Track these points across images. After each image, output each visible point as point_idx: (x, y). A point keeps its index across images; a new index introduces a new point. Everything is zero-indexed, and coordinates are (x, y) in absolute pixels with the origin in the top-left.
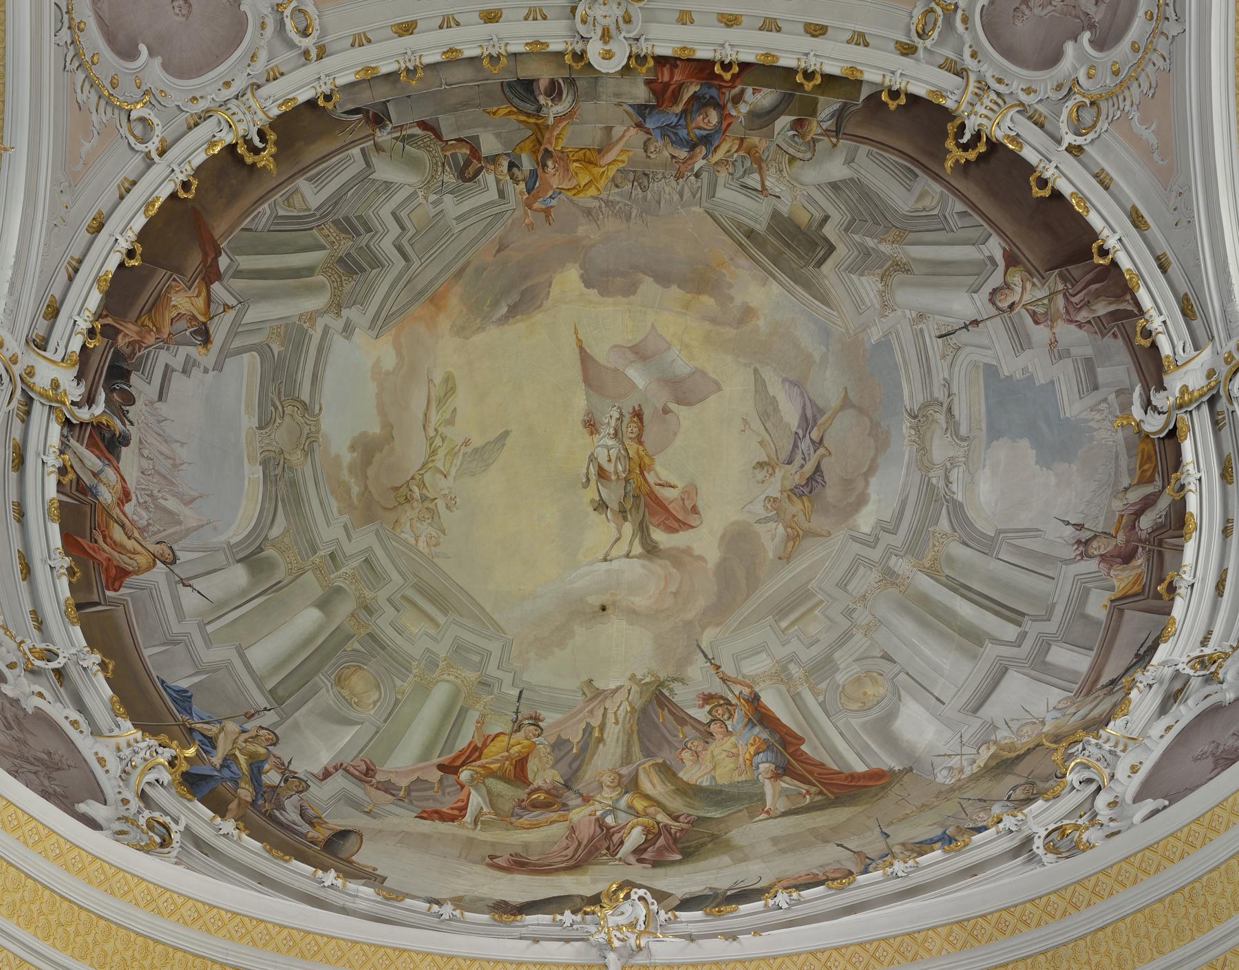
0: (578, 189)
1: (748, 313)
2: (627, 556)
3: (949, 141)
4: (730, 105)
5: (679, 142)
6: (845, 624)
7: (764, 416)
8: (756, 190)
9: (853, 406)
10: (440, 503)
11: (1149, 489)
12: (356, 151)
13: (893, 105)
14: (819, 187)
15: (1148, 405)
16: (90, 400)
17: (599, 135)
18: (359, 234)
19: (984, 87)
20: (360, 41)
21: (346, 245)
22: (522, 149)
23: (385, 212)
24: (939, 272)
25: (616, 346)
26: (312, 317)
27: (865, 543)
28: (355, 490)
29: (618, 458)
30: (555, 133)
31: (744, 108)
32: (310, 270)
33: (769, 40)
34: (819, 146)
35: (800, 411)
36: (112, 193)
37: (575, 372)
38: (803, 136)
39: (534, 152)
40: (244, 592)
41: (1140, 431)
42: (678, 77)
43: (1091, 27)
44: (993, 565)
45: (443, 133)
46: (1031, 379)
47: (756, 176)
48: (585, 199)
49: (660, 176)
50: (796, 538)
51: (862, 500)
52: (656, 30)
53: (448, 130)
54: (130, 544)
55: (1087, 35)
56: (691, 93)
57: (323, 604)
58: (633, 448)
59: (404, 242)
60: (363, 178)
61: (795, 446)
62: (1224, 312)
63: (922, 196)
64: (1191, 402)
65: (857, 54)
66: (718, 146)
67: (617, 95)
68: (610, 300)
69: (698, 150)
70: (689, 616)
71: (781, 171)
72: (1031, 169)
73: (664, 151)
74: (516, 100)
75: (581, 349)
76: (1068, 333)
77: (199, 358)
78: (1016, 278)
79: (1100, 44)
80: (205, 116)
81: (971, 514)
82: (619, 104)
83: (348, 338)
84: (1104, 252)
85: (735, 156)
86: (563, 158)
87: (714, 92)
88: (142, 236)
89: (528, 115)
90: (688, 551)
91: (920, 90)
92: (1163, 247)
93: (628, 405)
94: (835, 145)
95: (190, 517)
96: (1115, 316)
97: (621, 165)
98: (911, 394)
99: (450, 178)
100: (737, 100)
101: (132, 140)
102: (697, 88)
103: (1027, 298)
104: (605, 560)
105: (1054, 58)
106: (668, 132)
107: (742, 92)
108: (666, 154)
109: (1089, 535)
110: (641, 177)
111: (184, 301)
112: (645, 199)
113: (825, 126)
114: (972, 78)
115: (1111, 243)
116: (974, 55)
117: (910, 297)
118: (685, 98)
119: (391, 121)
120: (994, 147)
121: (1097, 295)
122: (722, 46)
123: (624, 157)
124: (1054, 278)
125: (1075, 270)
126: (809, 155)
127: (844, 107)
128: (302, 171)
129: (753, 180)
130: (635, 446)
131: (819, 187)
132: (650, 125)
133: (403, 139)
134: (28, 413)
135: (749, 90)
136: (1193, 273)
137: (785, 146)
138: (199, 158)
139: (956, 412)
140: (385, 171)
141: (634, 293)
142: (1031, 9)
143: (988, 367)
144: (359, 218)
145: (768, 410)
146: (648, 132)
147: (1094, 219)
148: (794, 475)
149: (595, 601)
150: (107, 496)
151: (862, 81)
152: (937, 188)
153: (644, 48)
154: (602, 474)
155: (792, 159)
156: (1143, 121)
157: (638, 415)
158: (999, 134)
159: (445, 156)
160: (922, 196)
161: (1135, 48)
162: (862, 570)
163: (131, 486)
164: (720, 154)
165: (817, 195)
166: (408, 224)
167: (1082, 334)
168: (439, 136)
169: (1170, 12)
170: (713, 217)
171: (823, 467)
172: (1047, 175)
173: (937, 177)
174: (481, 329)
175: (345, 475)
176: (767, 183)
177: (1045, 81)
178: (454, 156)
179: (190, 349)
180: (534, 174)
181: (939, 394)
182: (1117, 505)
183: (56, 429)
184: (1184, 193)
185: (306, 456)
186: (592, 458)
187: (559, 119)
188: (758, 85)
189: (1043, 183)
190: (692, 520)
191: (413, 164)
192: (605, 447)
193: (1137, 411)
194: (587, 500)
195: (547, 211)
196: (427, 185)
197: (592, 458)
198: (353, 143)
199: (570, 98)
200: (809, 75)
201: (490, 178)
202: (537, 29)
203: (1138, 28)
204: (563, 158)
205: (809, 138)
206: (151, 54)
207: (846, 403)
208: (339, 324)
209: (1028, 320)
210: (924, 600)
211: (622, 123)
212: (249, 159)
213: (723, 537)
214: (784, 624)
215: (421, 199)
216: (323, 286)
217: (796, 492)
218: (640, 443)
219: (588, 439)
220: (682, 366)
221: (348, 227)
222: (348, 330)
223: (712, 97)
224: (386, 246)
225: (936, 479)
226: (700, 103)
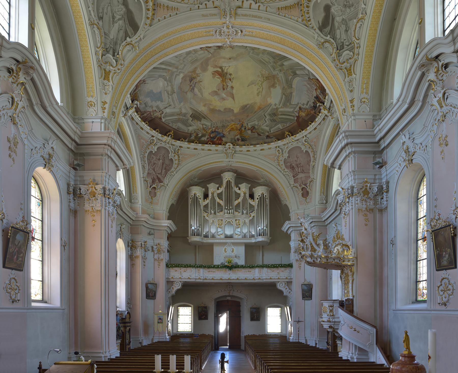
0: (234, 124)
1: (205, 106)
2: (225, 67)
5: (217, 132)
6: (184, 60)
7: (201, 89)
9: (185, 92)
10: (260, 76)
11: (135, 93)
12: (272, 132)
13: (182, 139)
14: (193, 126)
15: (137, 105)
16: (319, 106)
18: (272, 119)
19: (168, 143)
20: (270, 148)
21: (275, 118)
23: (268, 122)
24: (172, 115)
25: (228, 100)
26: (281, 108)
27: (181, 72)
28: (276, 80)
29: (227, 82)
31: (207, 137)
32: (281, 115)
33: (203, 148)
35: (194, 91)
36: (312, 133)
37: (235, 96)
39: (242, 130)
40: (297, 70)
41: (137, 100)
42: (218, 141)
43: (153, 154)
44: (159, 74)
46: (155, 102)
47: (204, 127)
48: (233, 123)
50: (194, 71)
51: (182, 78)
52: (221, 149)
53: (256, 135)
54: (316, 83)
55: (154, 153)
57: (283, 65)
58: (225, 84)
59: (265, 118)
60: (271, 128)
61: (195, 85)
62: (128, 121)
63: (176, 125)
64: (131, 108)
65: (189, 146)
67: (228, 139)
68: (229, 107)
70: (214, 58)
72: (159, 133)
73: (220, 130)
74: (245, 138)
75: (234, 100)
76: (150, 110)
77: (302, 105)
78: (159, 116)
79: (151, 152)
80: (296, 141)
81: (163, 80)
83: (275, 103)
84: (146, 123)
86: (237, 129)
87: (212, 139)
88: (308, 126)
89: (242, 136)
90: (214, 68)
91: (178, 142)
92: (137, 126)
93: (225, 91)
95: (305, 83)
96: (143, 114)
98: (175, 96)
99: (256, 127)
100: (208, 138)
101: (308, 139)
103: (157, 113)
104: (230, 66)
106: (219, 133)
109: (144, 83)
110: (223, 126)
111: (303, 114)
112: (223, 123)
114: (170, 144)
115: (146, 125)
116: (170, 147)
117: (177, 110)
120: (165, 135)
121: (146, 116)
123: (226, 129)
124: (153, 117)
125: (150, 119)
128: (281, 130)
129: (204, 126)
130: (224, 84)
131: (193, 126)
134: (330, 107)
135: (206, 140)
136: (133, 124)
138: (297, 135)
139: (167, 94)
140: (267, 129)
141: (225, 109)
143: (163, 102)
144: (272, 122)
145: (200, 90)
147: (149, 128)
148: (195, 81)
149: (231, 60)
150: (319, 91)
151: (188, 142)
152: (174, 127)
153: (223, 146)
154: (230, 80)
156: (143, 142)
157: (224, 89)
158: (166, 137)
160: (176, 125)
161: (146, 152)
162: (182, 68)
163: (315, 91)
164: (210, 130)
165: (194, 124)
166: (264, 120)
167: (148, 110)
168: (258, 133)
169: (142, 158)
170: (211, 120)
171: (190, 83)
172: (157, 133)
173: (174, 129)
174: (252, 103)
175: (278, 83)
177: (159, 145)
178: (255, 130)
179: (303, 107)
180: (242, 127)
181: (170, 97)
182: (139, 88)
183: (325, 104)
184: (136, 134)
185: (284, 87)
186: (232, 82)
187: (237, 135)
188: (204, 141)
189: (157, 131)
190: (213, 73)
191: (262, 129)
192: (230, 84)
193: (138, 103)
194: (233, 75)
195: (240, 121)
196: (260, 126)
197: (232, 82)
198: (272, 133)
200: (196, 143)
201: (249, 127)
202: (241, 149)
203: (146, 155)
206: (303, 151)
207: (186, 93)
208: (277, 106)
209: (157, 110)
210: (170, 66)
212: (290, 133)
213: (208, 70)
214: (196, 58)
215: (261, 124)
216: (279, 112)
217: (194, 78)
218: (223, 85)
219: (233, 85)
220: (216, 97)
221: (274, 121)
222: (275, 105)
224: (268, 117)
225: (170, 84)
226: (214, 138)
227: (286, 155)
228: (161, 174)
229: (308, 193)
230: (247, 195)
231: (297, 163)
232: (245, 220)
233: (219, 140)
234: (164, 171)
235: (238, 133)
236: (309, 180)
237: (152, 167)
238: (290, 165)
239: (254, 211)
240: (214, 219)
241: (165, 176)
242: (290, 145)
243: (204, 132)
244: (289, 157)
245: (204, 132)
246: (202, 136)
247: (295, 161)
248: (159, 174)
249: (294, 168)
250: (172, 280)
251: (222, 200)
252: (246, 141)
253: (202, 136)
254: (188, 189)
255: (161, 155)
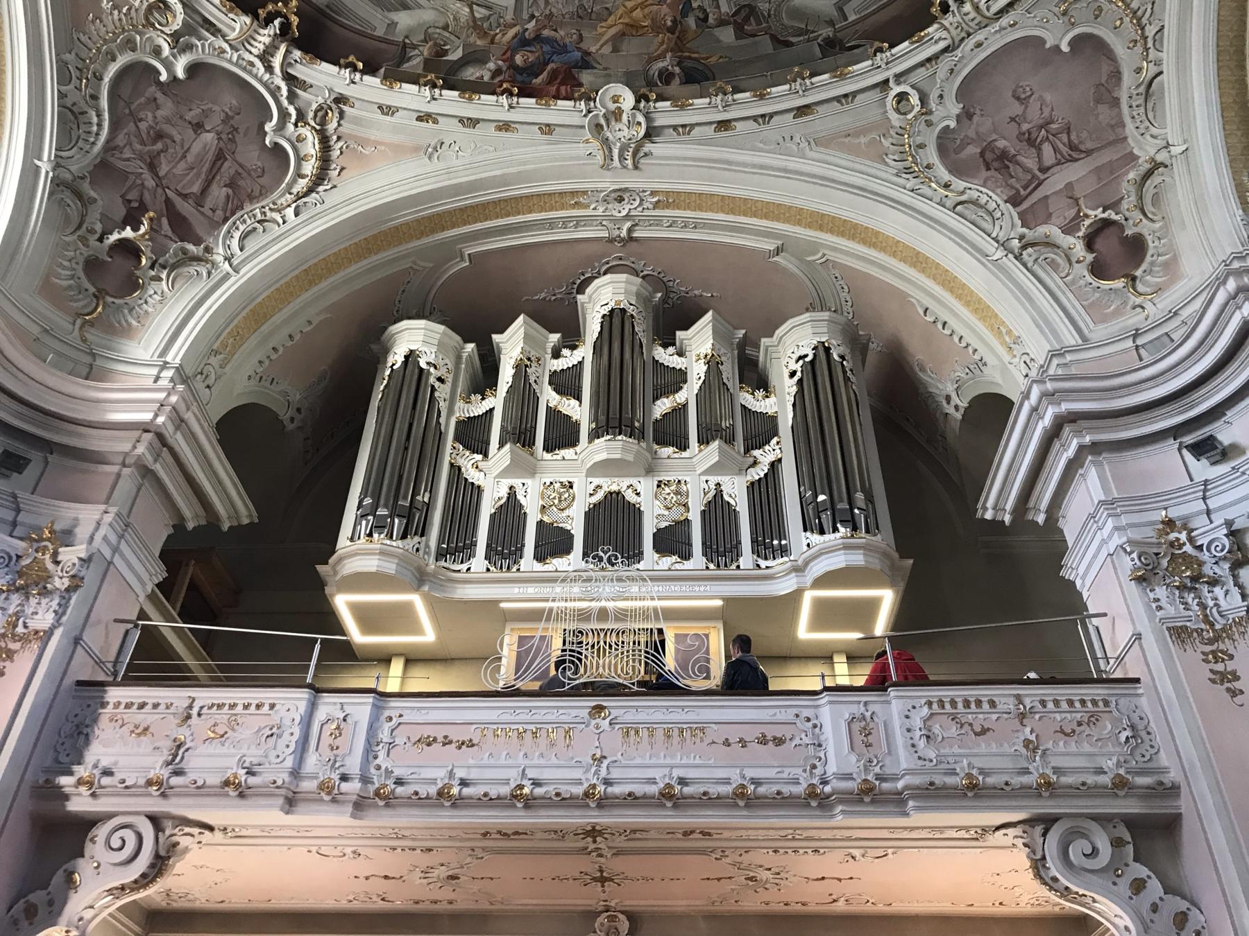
3: (296, 23)
4: (504, 69)
5: (548, 41)
8: (478, 5)
12: (852, 18)
13: (352, 58)
17: (624, 46)
22: (695, 32)
30: (665, 46)
31: (491, 65)
34: (422, 37)
38: (435, 44)
39: (684, 31)
43: (159, 83)
45: (769, 41)
47: (477, 15)
49: (567, 16)
56: (541, 77)
66: (514, 38)
69: (532, 36)
71: (455, 19)
82: (605, 69)
85: (498, 31)
86: (657, 27)
87: (519, 78)
89: (690, 58)
94: (407, 37)
97: (603, 24)
102: (534, 81)
105: (193, 69)
106: (562, 49)
107: (493, 77)
108: (562, 33)
110: (584, 16)
113: (416, 52)
118: (545, 73)
119: (819, 45)
122: (511, 107)
123: (600, 30)
126: (430, 31)
127: (399, 64)
132: (578, 54)
133: (807, 32)
135: (486, 79)
137: (452, 37)
142: (223, 111)
146: (579, 49)
155: (446, 28)
159: (768, 22)
164: (512, 33)
168: (774, 38)
176: (468, 10)
180: (684, 14)
187: (662, 57)
199: (651, 72)
201: (725, 8)
204: (657, 27)
205: (431, 43)
211: (602, 56)
223: (521, 74)
227: (948, 113)
228: (199, 200)
229: (1136, 248)
230: (729, 371)
231: (1025, 127)
232: (718, 484)
233: (561, 84)
234: (218, 193)
235: (663, 42)
236: (1131, 175)
237: (143, 143)
238: (982, 154)
239: (776, 434)
240: (517, 482)
241: (226, 220)
242: (970, 58)
243: (479, 42)
244: (966, 115)
245: (479, 42)
246: (465, 61)
247: (1013, 119)
248: (185, 196)
249: (1012, 159)
250: (80, 804)
251: (579, 398)
252: (707, 79)
253: (465, 61)
254: (374, 347)
255: (216, 108)
